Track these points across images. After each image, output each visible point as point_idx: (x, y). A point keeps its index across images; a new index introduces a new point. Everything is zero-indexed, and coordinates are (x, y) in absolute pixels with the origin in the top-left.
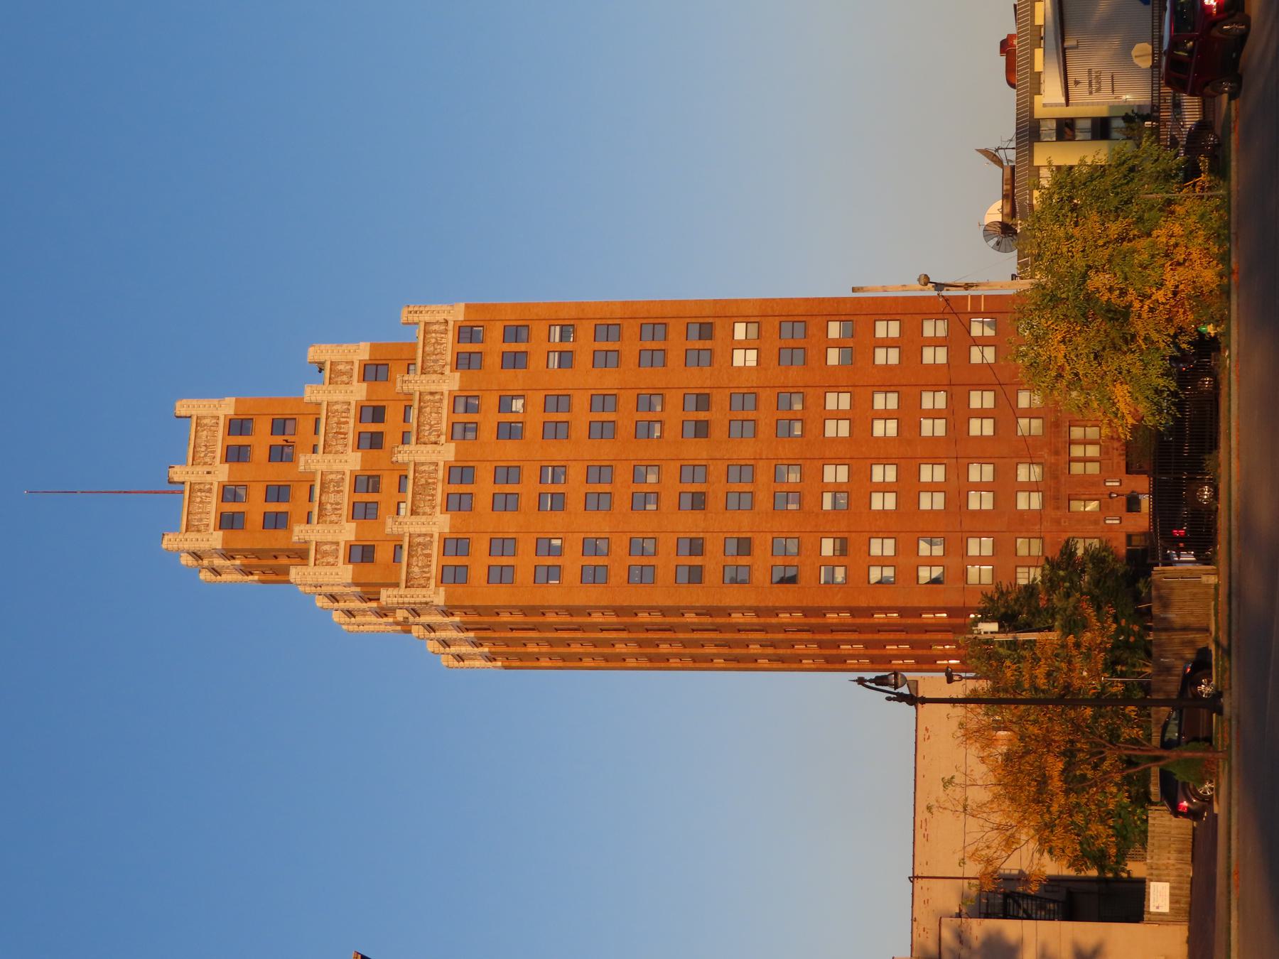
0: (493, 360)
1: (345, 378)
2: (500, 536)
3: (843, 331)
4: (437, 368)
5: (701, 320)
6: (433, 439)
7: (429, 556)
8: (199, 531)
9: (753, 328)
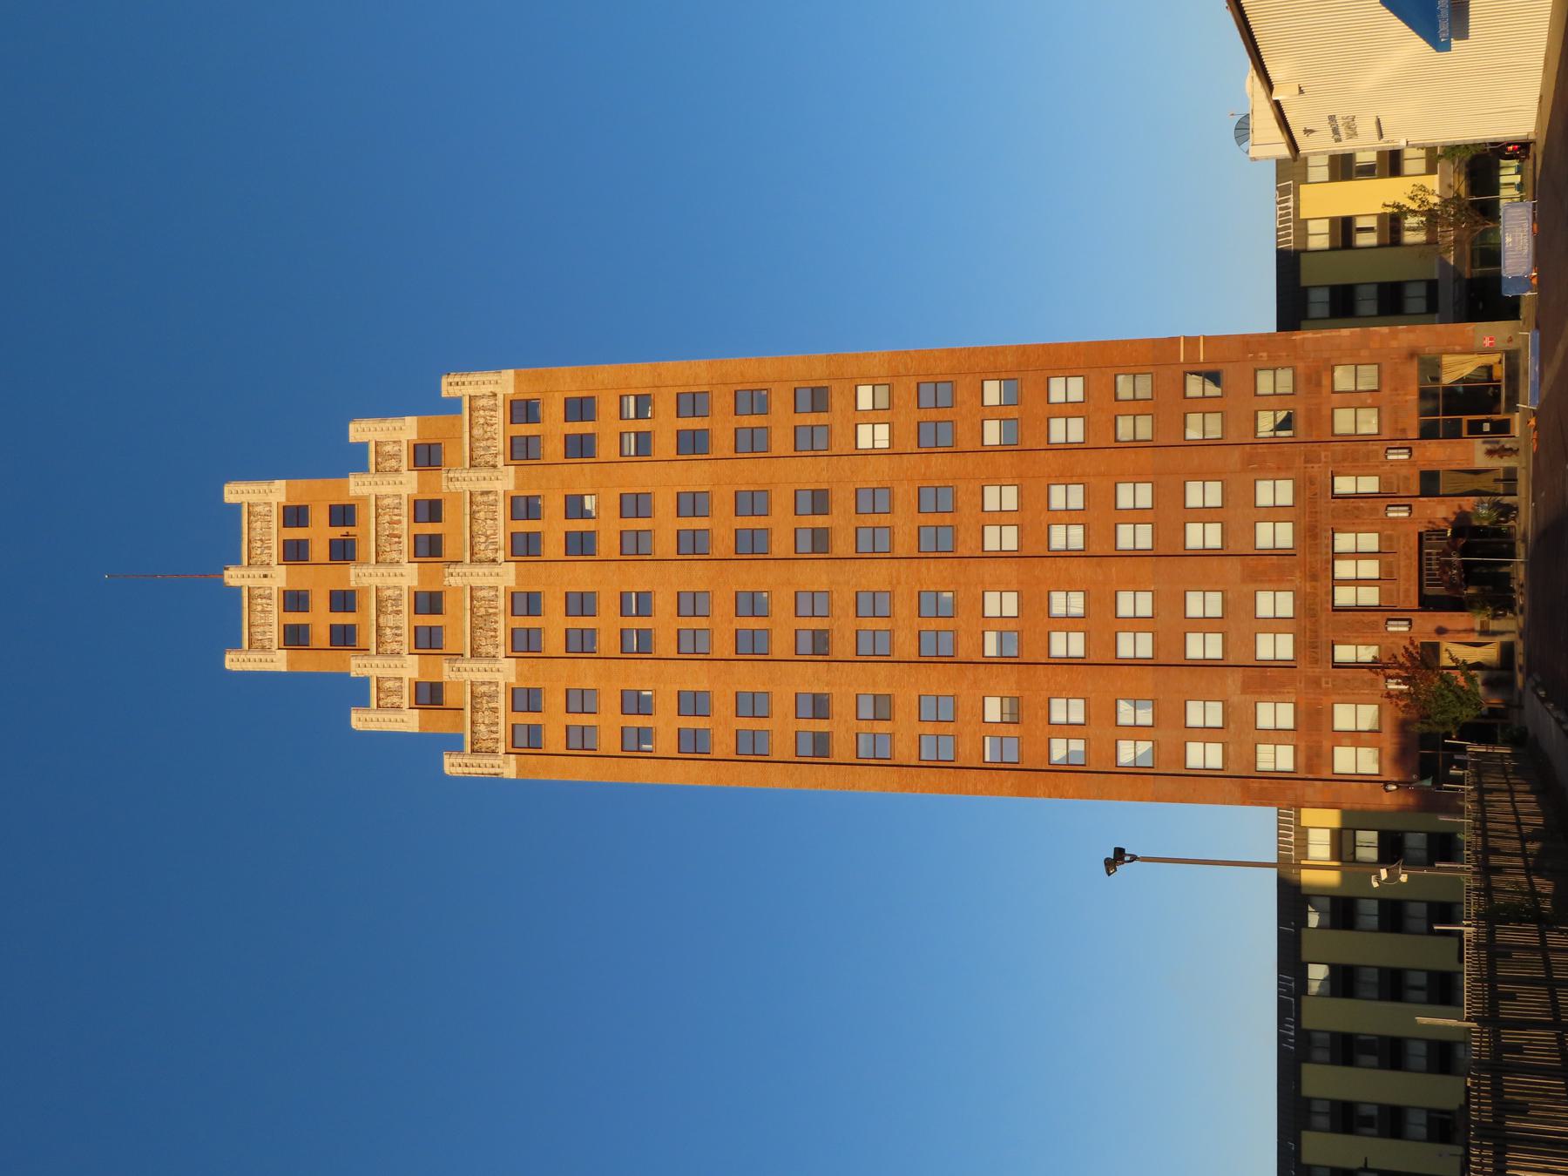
0: (554, 449)
1: (393, 463)
2: (749, 387)
3: (1004, 393)
4: (488, 458)
5: (813, 384)
6: (491, 555)
7: (494, 710)
8: (263, 648)
9: (883, 392)
